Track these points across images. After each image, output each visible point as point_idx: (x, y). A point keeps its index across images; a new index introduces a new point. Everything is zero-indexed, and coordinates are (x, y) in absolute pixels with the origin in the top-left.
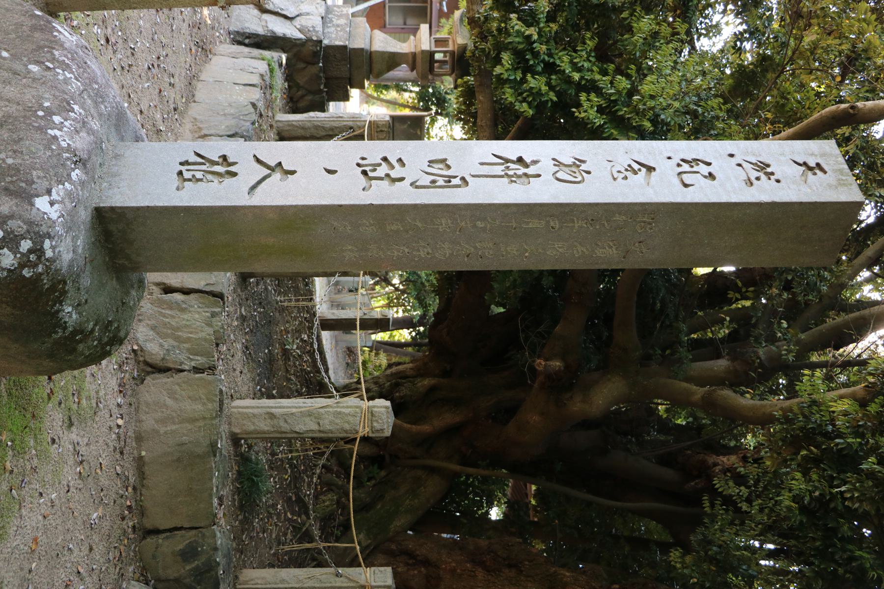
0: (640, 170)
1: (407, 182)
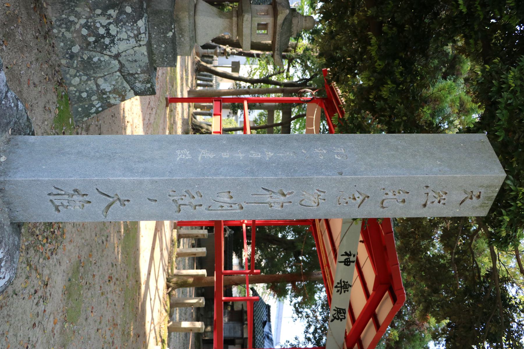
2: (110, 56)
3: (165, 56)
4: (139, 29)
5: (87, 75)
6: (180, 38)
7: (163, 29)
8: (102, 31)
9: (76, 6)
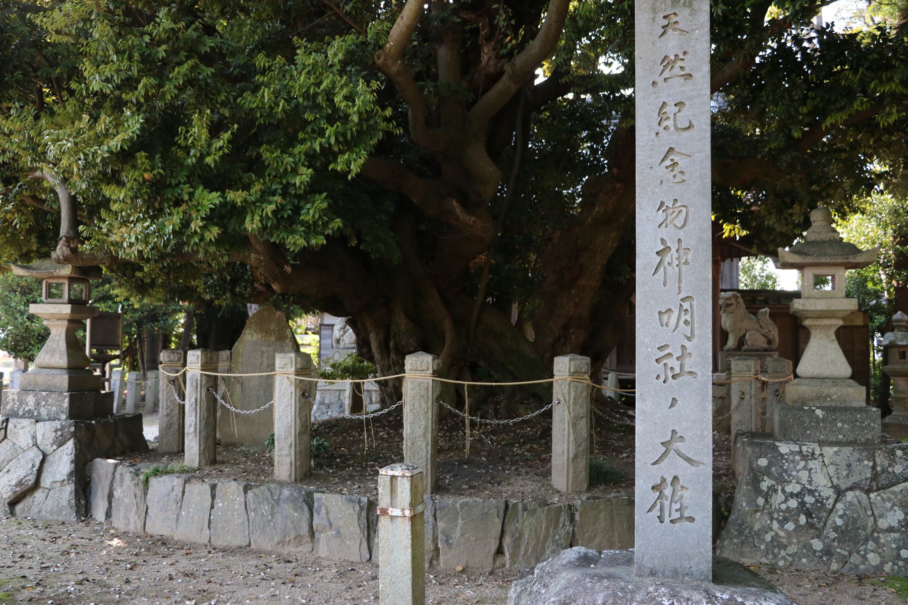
0: (672, 160)
1: (687, 344)
2: (836, 501)
3: (858, 424)
4: (792, 453)
5: (866, 541)
6: (832, 400)
7: (810, 422)
8: (793, 503)
9: (751, 529)
